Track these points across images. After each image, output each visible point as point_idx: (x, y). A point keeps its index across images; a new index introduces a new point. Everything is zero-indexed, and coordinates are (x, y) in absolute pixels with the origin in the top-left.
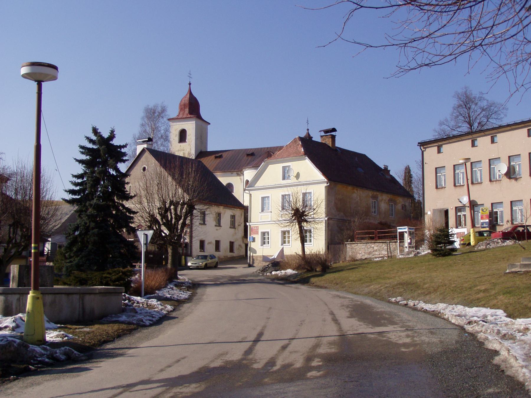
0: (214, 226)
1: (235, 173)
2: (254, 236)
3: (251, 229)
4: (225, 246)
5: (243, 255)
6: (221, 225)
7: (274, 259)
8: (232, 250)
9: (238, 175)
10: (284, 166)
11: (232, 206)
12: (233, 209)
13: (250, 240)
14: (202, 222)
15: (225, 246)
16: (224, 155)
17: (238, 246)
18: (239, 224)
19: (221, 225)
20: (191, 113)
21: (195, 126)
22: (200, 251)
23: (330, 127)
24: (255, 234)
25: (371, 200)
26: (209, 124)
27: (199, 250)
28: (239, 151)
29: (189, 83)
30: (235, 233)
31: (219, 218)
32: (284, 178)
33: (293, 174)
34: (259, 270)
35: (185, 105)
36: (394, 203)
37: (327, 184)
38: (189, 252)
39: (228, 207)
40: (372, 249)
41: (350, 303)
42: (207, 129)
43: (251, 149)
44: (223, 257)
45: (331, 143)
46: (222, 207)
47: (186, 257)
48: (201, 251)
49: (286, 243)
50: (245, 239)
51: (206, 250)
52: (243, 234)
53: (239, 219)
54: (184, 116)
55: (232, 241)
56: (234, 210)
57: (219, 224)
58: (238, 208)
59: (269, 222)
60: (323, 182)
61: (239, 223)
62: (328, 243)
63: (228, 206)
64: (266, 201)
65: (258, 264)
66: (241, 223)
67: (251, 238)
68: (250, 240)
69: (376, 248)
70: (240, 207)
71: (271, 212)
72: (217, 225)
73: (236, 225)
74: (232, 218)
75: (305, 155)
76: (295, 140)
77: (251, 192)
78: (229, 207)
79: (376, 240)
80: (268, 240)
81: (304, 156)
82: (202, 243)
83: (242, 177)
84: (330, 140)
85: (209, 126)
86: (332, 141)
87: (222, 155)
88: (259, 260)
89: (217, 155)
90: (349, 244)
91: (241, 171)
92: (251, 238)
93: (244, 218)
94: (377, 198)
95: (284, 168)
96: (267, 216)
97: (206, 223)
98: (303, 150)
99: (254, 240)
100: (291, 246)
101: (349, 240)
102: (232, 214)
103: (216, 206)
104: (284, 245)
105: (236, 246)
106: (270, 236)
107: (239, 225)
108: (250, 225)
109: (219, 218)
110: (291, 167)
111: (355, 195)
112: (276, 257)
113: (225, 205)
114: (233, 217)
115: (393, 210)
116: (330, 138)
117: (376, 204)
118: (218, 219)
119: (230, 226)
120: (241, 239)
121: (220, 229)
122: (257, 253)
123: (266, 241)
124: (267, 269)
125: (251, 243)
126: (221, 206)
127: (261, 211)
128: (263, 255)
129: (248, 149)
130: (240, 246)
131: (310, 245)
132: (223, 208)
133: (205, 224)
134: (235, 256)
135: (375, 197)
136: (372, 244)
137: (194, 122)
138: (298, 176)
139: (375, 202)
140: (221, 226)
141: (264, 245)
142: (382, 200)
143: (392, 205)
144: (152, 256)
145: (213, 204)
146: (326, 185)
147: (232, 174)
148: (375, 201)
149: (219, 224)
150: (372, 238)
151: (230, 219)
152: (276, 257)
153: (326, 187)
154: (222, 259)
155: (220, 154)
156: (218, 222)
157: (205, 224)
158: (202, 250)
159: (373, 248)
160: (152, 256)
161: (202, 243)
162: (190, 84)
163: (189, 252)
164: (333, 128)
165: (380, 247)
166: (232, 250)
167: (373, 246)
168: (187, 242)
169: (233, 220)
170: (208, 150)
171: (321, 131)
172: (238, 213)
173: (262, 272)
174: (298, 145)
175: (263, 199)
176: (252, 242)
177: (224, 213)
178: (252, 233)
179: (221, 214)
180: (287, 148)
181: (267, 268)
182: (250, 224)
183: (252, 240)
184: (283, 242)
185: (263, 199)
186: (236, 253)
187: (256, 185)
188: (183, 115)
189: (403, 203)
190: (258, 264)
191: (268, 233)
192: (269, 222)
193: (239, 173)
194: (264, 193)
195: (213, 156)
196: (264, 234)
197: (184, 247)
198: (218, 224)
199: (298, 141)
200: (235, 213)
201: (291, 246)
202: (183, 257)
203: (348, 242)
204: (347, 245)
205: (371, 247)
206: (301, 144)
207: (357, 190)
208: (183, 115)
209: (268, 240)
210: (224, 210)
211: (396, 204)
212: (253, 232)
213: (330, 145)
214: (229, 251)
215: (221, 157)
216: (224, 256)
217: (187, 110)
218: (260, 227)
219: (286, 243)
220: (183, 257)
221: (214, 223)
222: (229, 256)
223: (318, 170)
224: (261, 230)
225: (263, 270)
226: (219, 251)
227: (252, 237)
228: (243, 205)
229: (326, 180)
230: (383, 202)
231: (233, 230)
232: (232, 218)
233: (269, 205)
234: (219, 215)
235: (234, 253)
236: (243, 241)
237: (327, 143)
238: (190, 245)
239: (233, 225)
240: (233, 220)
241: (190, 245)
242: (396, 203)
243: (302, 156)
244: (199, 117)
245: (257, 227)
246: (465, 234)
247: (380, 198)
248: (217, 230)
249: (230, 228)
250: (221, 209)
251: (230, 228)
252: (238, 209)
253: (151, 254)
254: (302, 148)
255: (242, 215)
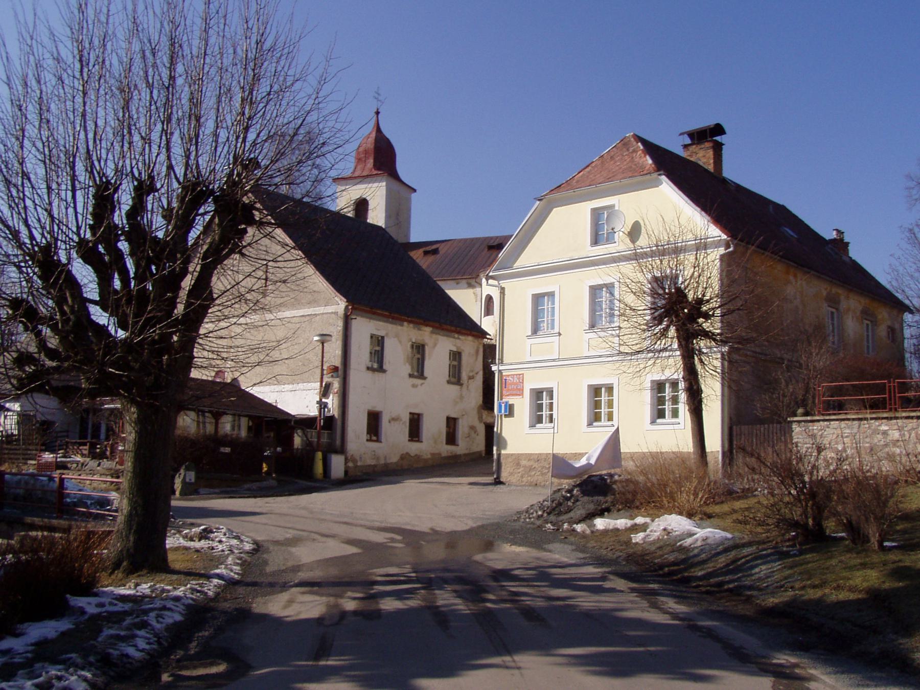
0: (408, 376)
1: (464, 281)
2: (511, 400)
3: (504, 383)
4: (433, 427)
5: (480, 453)
6: (426, 374)
7: (588, 466)
8: (451, 439)
9: (470, 286)
10: (554, 295)
11: (453, 328)
12: (456, 336)
13: (500, 410)
14: (375, 366)
15: (433, 427)
16: (443, 249)
17: (466, 430)
18: (471, 374)
19: (426, 374)
20: (378, 165)
21: (385, 192)
22: (367, 440)
23: (708, 122)
24: (513, 395)
25: (826, 309)
26: (415, 191)
27: (364, 436)
28: (472, 242)
29: (375, 110)
30: (461, 397)
31: (419, 356)
32: (596, 241)
33: (622, 227)
34: (541, 507)
35: (366, 152)
36: (872, 322)
37: (728, 247)
38: (338, 442)
39: (443, 329)
40: (880, 436)
41: (756, 573)
42: (409, 200)
43: (497, 237)
44: (429, 456)
45: (712, 161)
46: (428, 329)
47: (328, 455)
48: (369, 440)
49: (600, 420)
50: (485, 414)
51: (383, 438)
52: (481, 398)
53: (472, 363)
54: (365, 174)
55: (453, 415)
56: (459, 338)
57: (419, 372)
58: (468, 335)
59: (554, 360)
60: (717, 245)
61: (472, 371)
62: (730, 419)
63: (445, 327)
64: (546, 305)
65: (522, 477)
66: (477, 374)
67: (503, 405)
68: (500, 410)
69: (896, 435)
70: (475, 333)
71: (560, 334)
72: (416, 374)
73: (464, 376)
74: (454, 359)
75: (658, 170)
76: (624, 143)
77: (503, 283)
78: (447, 330)
79: (890, 410)
80: (548, 413)
81: (655, 175)
82: (374, 421)
83: (478, 289)
84: (711, 153)
85: (414, 195)
86: (714, 154)
87: (438, 249)
88: (525, 467)
89: (429, 248)
90: (799, 422)
91: (476, 278)
92: (503, 405)
93: (484, 382)
94: (838, 302)
95: (596, 214)
96: (546, 347)
97: (385, 367)
98: (650, 161)
99: (510, 411)
100: (681, 426)
101: (800, 411)
102: (455, 349)
103: (411, 325)
104: (595, 424)
105: (462, 429)
106: (555, 401)
107: (471, 378)
108: (500, 371)
109: (419, 356)
110: (616, 208)
111: (790, 290)
112: (593, 461)
113: (437, 325)
114: (456, 356)
115: (870, 337)
116: (708, 148)
117: (835, 319)
118: (418, 359)
119: (447, 378)
120: (475, 412)
121: (422, 384)
122: (508, 447)
123: (545, 413)
124: (570, 503)
125: (503, 418)
126: (427, 325)
127: (530, 334)
128: (553, 454)
129: (491, 238)
130: (472, 428)
131: (676, 427)
132: (432, 332)
133: (384, 371)
134: (459, 453)
135: (833, 301)
136: (880, 421)
137: (384, 184)
138: (634, 232)
139: (832, 313)
140: (425, 378)
141: (538, 426)
142: (849, 310)
143: (867, 325)
144: (227, 450)
145: (406, 321)
146: (722, 251)
147: (457, 283)
148: (834, 310)
149: (419, 372)
150: (875, 406)
151: (448, 362)
152: (593, 461)
153: (722, 257)
154: (426, 460)
155: (434, 247)
156: (418, 365)
157: (384, 371)
158: (374, 438)
159: (885, 433)
160: (227, 450)
161: (374, 421)
162: (378, 113)
163: (338, 442)
164: (715, 123)
165: (909, 432)
166: (451, 439)
167: (884, 428)
168: (332, 417)
169: (455, 363)
170: (412, 241)
171: (681, 134)
172: (468, 345)
173: (552, 518)
174: (635, 151)
175: (538, 299)
176: (506, 416)
177: (435, 345)
178: (504, 392)
179: (426, 347)
180: (602, 163)
181: (568, 499)
182: (501, 368)
183: (505, 411)
184: (593, 417)
185: (538, 299)
186: (462, 447)
187: (517, 264)
188: (363, 170)
189: (889, 323)
190: (522, 477)
191: (550, 392)
192: (554, 360)
193: (473, 282)
194: (540, 285)
195: (421, 251)
196: (538, 394)
197: (323, 428)
198: (418, 371)
199: (635, 143)
200: (462, 348)
201: (681, 426)
202: (319, 455)
203: (796, 416)
204: (794, 426)
205: (876, 432)
206: (642, 147)
207: (795, 276)
208: (363, 170)
209: (548, 413)
210: (434, 336)
211: (876, 325)
212: (508, 390)
213: (711, 168)
214: (444, 442)
215: (435, 252)
216: (432, 454)
217: (370, 162)
218: (528, 375)
219: (600, 420)
220: (319, 455)
221: (407, 369)
222: (444, 454)
223: (699, 209)
224: (532, 382)
225: (554, 509)
226: (419, 441)
227: (507, 402)
228: (480, 327)
229: (724, 237)
230: (850, 316)
231: (455, 388)
232: (454, 359)
233: (553, 315)
234: (419, 349)
235: (458, 445)
236: (480, 418)
237: (701, 163)
238: (339, 423)
239: (455, 376)
240: (455, 363)
241: (339, 423)
242: (875, 323)
243: (650, 173)
244: (393, 174)
245: (521, 377)
246: (184, 467)
247: (844, 305)
248: (414, 386)
249: (449, 382)
250: (425, 334)
251: (449, 382)
252: (470, 338)
253: (225, 445)
254: (648, 157)
255: (477, 352)
